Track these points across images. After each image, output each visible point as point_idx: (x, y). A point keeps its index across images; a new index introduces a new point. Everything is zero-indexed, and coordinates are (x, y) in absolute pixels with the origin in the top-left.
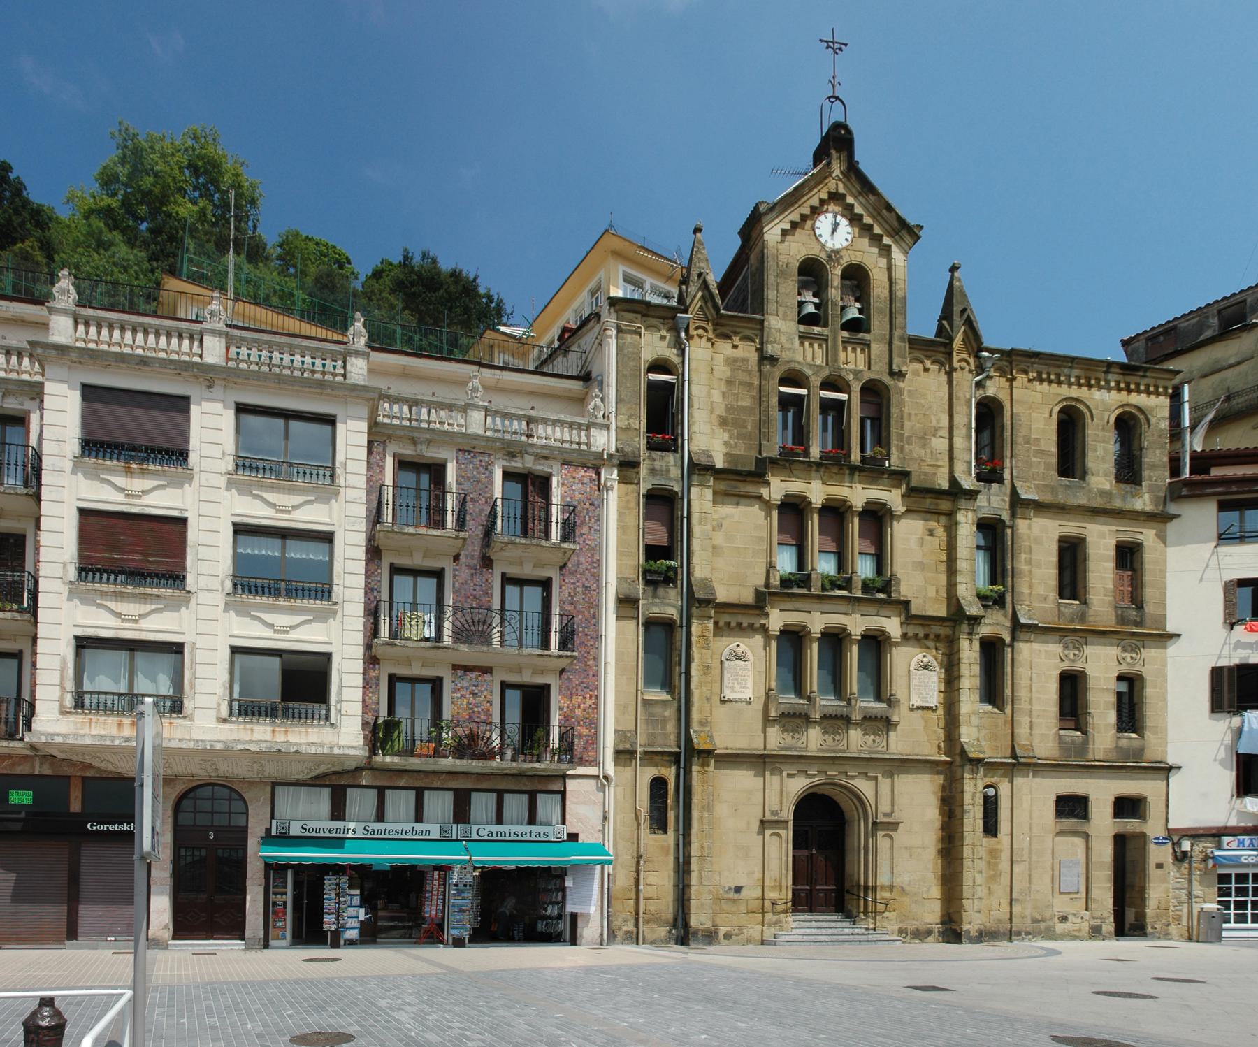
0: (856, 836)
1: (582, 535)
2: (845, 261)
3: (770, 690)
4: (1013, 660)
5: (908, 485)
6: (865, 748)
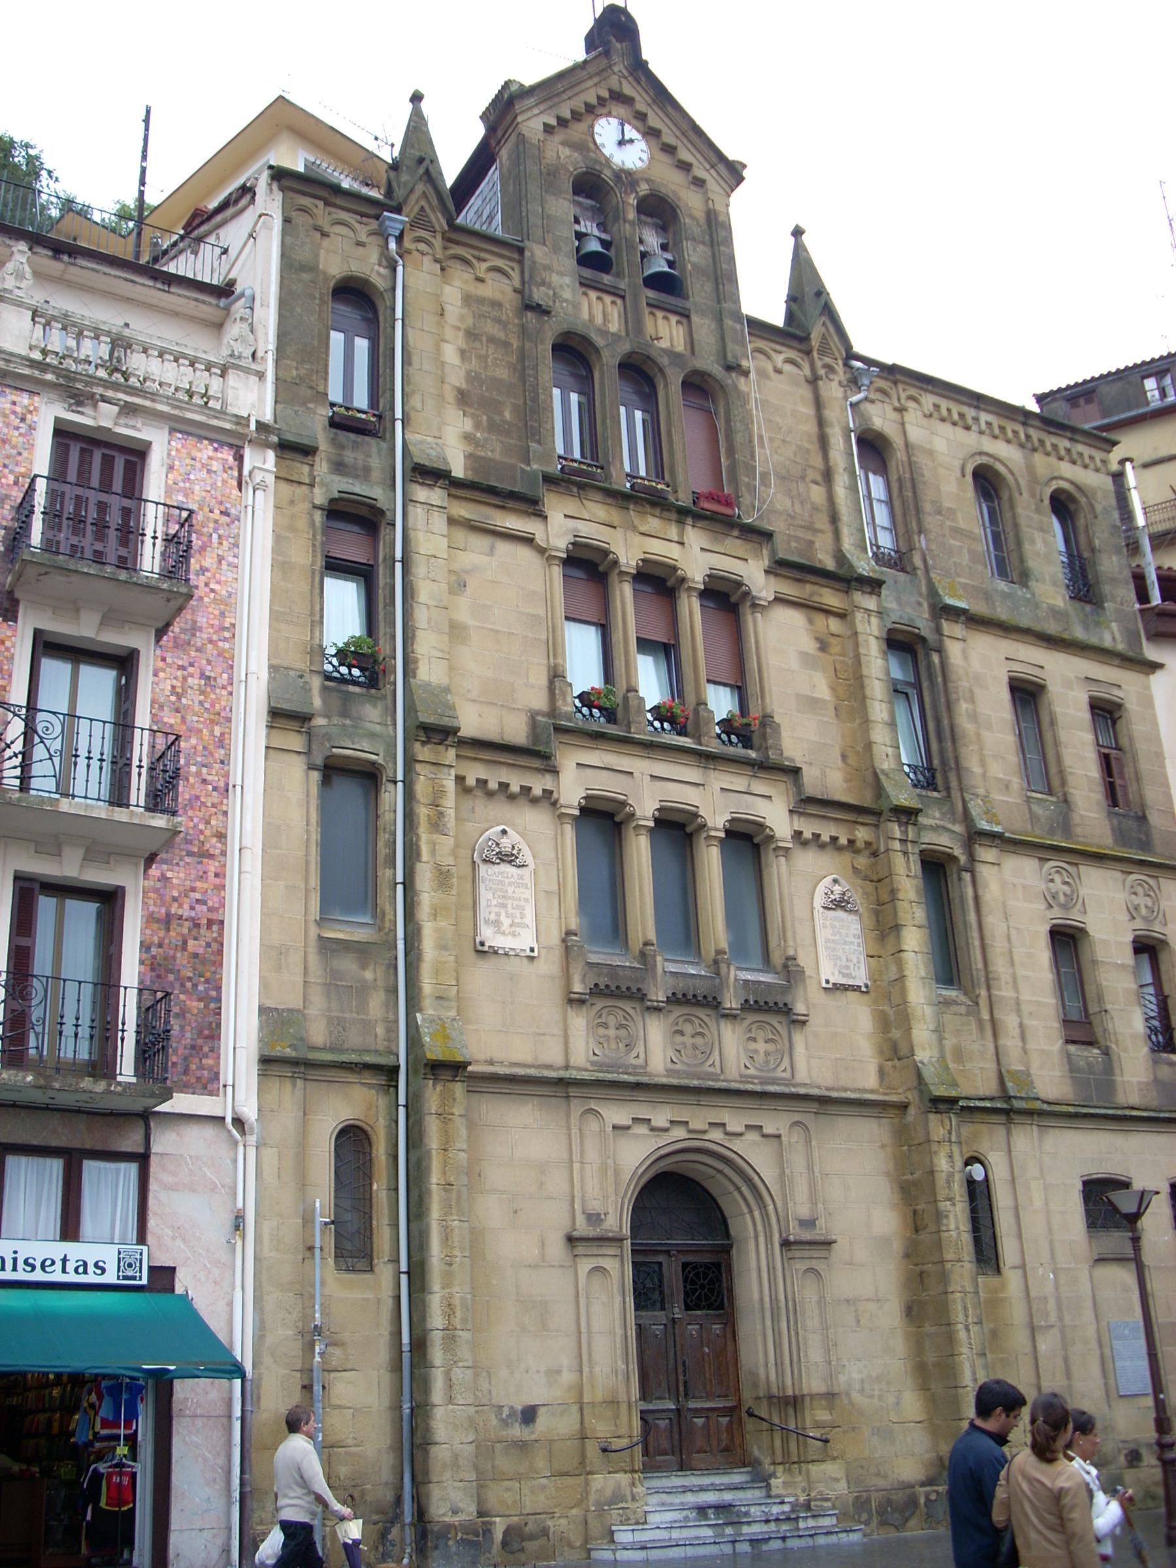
0: (754, 1275)
1: (203, 570)
2: (644, 189)
3: (569, 933)
4: (977, 898)
5: (773, 552)
6: (752, 1072)
